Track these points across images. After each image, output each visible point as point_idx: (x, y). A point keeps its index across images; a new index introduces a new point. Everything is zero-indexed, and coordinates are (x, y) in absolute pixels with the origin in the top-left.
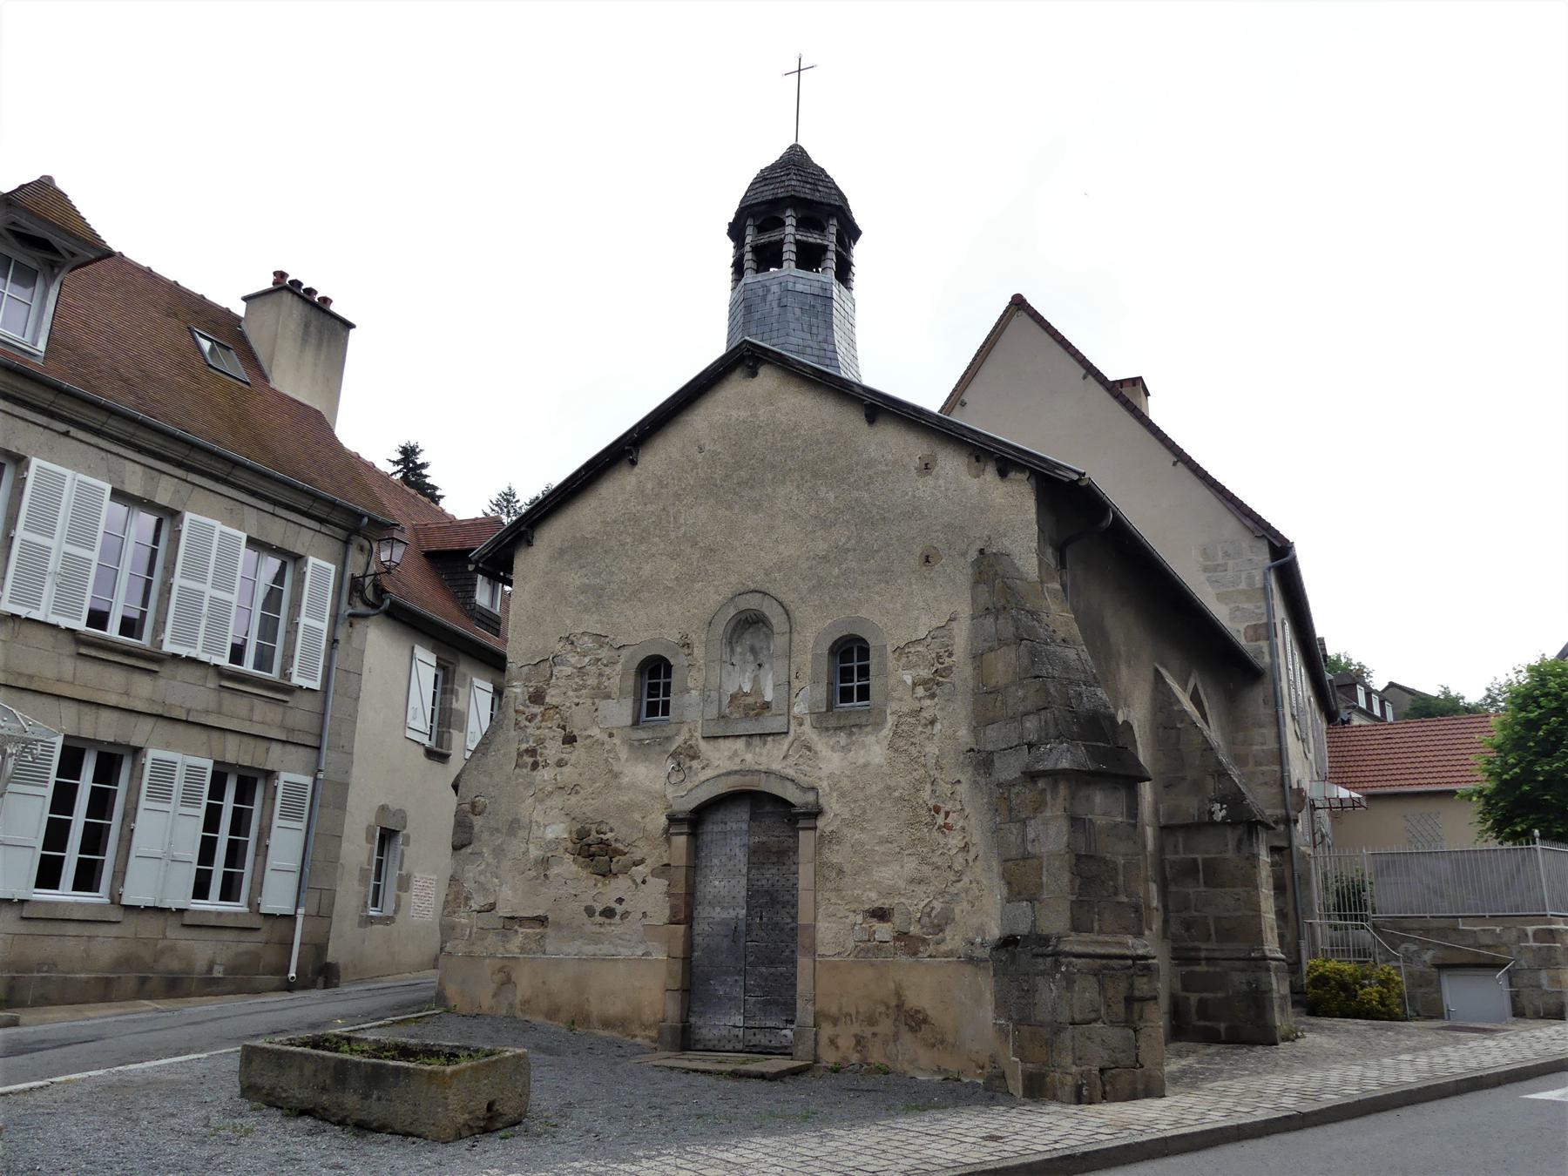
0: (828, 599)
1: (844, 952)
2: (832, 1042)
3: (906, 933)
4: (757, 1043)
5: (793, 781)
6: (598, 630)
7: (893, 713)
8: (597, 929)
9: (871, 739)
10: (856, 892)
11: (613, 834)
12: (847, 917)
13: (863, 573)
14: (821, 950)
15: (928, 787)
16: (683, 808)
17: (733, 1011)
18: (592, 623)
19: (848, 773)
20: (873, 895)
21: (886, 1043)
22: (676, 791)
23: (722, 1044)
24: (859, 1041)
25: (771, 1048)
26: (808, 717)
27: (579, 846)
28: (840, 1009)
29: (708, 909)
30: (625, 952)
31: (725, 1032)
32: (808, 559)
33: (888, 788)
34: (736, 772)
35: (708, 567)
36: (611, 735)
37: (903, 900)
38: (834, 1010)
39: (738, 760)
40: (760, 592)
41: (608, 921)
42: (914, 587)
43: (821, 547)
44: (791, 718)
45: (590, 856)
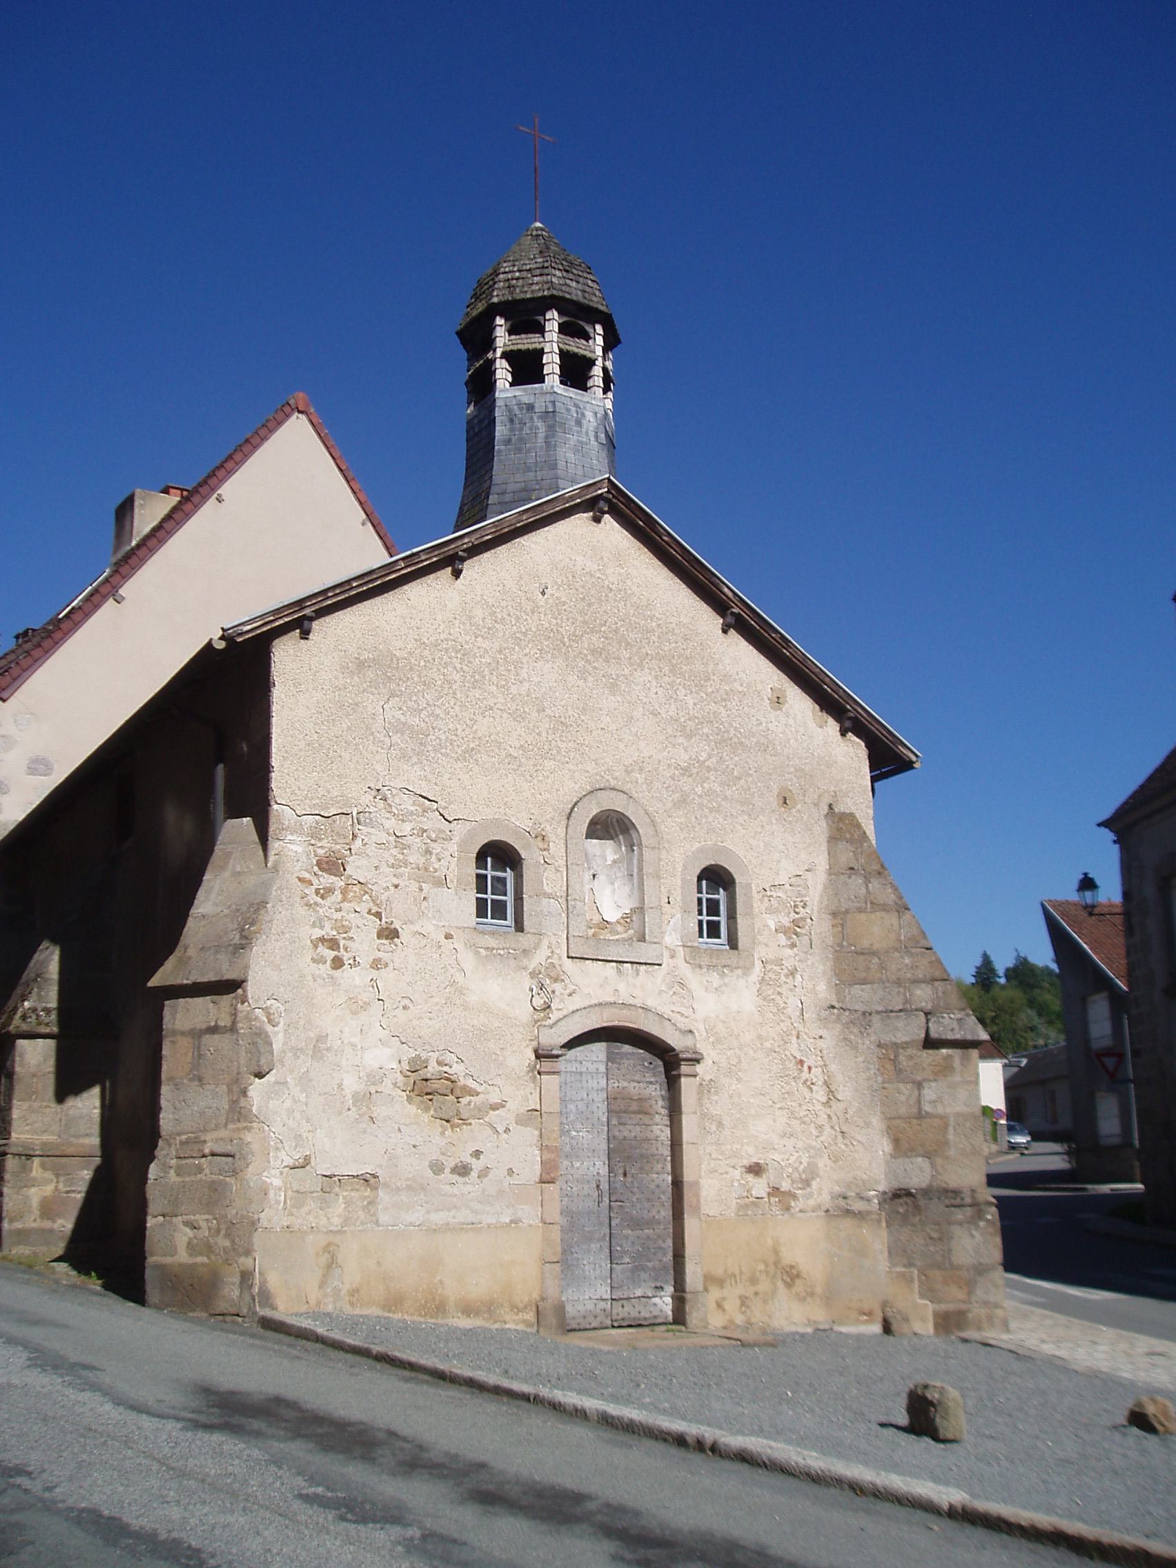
9: (741, 983)
12: (726, 1173)
18: (413, 776)
20: (751, 1150)
24: (744, 1301)
28: (725, 1271)
31: (590, 1306)
33: (760, 1037)
38: (719, 1272)
43: (682, 757)
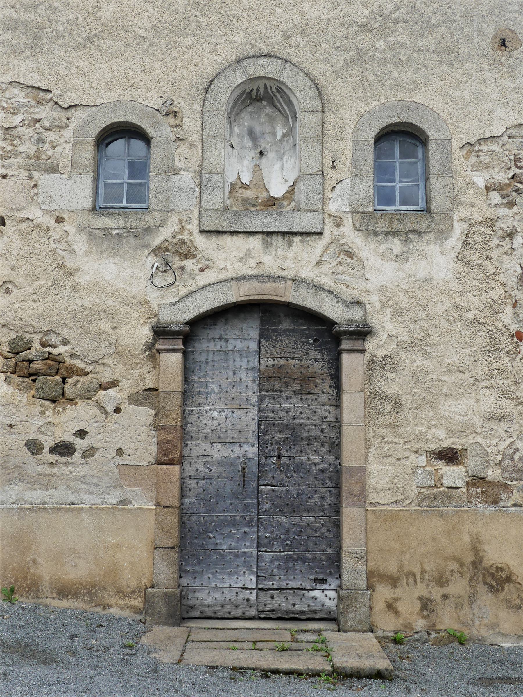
0: (372, 77)
1: (403, 500)
2: (390, 607)
3: (481, 478)
4: (275, 607)
5: (330, 292)
6: (37, 81)
7: (462, 220)
8: (48, 470)
9: (433, 249)
10: (419, 429)
11: (67, 348)
12: (406, 458)
13: (418, 50)
14: (373, 497)
15: (509, 309)
16: (175, 319)
17: (242, 570)
19: (406, 287)
20: (441, 433)
21: (459, 606)
22: (162, 297)
23: (227, 609)
25: (293, 612)
26: (349, 216)
27: (13, 361)
28: (401, 567)
29: (203, 445)
30: (90, 500)
32: (342, 25)
33: (458, 307)
34: (251, 277)
35: (200, 18)
36: (60, 220)
37: (479, 439)
38: (392, 569)
39: (252, 263)
40: (278, 58)
41: (63, 459)
42: (487, 73)
44: (326, 216)
45: (31, 375)
